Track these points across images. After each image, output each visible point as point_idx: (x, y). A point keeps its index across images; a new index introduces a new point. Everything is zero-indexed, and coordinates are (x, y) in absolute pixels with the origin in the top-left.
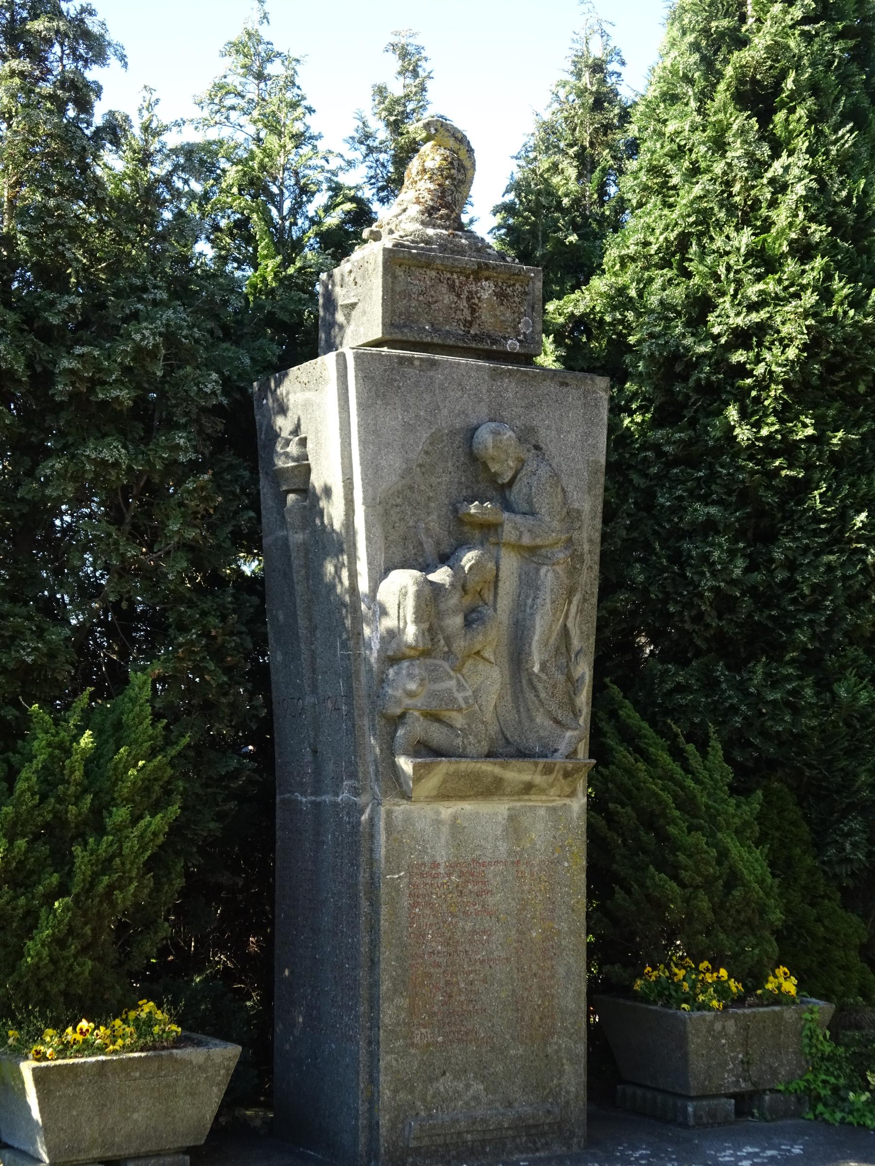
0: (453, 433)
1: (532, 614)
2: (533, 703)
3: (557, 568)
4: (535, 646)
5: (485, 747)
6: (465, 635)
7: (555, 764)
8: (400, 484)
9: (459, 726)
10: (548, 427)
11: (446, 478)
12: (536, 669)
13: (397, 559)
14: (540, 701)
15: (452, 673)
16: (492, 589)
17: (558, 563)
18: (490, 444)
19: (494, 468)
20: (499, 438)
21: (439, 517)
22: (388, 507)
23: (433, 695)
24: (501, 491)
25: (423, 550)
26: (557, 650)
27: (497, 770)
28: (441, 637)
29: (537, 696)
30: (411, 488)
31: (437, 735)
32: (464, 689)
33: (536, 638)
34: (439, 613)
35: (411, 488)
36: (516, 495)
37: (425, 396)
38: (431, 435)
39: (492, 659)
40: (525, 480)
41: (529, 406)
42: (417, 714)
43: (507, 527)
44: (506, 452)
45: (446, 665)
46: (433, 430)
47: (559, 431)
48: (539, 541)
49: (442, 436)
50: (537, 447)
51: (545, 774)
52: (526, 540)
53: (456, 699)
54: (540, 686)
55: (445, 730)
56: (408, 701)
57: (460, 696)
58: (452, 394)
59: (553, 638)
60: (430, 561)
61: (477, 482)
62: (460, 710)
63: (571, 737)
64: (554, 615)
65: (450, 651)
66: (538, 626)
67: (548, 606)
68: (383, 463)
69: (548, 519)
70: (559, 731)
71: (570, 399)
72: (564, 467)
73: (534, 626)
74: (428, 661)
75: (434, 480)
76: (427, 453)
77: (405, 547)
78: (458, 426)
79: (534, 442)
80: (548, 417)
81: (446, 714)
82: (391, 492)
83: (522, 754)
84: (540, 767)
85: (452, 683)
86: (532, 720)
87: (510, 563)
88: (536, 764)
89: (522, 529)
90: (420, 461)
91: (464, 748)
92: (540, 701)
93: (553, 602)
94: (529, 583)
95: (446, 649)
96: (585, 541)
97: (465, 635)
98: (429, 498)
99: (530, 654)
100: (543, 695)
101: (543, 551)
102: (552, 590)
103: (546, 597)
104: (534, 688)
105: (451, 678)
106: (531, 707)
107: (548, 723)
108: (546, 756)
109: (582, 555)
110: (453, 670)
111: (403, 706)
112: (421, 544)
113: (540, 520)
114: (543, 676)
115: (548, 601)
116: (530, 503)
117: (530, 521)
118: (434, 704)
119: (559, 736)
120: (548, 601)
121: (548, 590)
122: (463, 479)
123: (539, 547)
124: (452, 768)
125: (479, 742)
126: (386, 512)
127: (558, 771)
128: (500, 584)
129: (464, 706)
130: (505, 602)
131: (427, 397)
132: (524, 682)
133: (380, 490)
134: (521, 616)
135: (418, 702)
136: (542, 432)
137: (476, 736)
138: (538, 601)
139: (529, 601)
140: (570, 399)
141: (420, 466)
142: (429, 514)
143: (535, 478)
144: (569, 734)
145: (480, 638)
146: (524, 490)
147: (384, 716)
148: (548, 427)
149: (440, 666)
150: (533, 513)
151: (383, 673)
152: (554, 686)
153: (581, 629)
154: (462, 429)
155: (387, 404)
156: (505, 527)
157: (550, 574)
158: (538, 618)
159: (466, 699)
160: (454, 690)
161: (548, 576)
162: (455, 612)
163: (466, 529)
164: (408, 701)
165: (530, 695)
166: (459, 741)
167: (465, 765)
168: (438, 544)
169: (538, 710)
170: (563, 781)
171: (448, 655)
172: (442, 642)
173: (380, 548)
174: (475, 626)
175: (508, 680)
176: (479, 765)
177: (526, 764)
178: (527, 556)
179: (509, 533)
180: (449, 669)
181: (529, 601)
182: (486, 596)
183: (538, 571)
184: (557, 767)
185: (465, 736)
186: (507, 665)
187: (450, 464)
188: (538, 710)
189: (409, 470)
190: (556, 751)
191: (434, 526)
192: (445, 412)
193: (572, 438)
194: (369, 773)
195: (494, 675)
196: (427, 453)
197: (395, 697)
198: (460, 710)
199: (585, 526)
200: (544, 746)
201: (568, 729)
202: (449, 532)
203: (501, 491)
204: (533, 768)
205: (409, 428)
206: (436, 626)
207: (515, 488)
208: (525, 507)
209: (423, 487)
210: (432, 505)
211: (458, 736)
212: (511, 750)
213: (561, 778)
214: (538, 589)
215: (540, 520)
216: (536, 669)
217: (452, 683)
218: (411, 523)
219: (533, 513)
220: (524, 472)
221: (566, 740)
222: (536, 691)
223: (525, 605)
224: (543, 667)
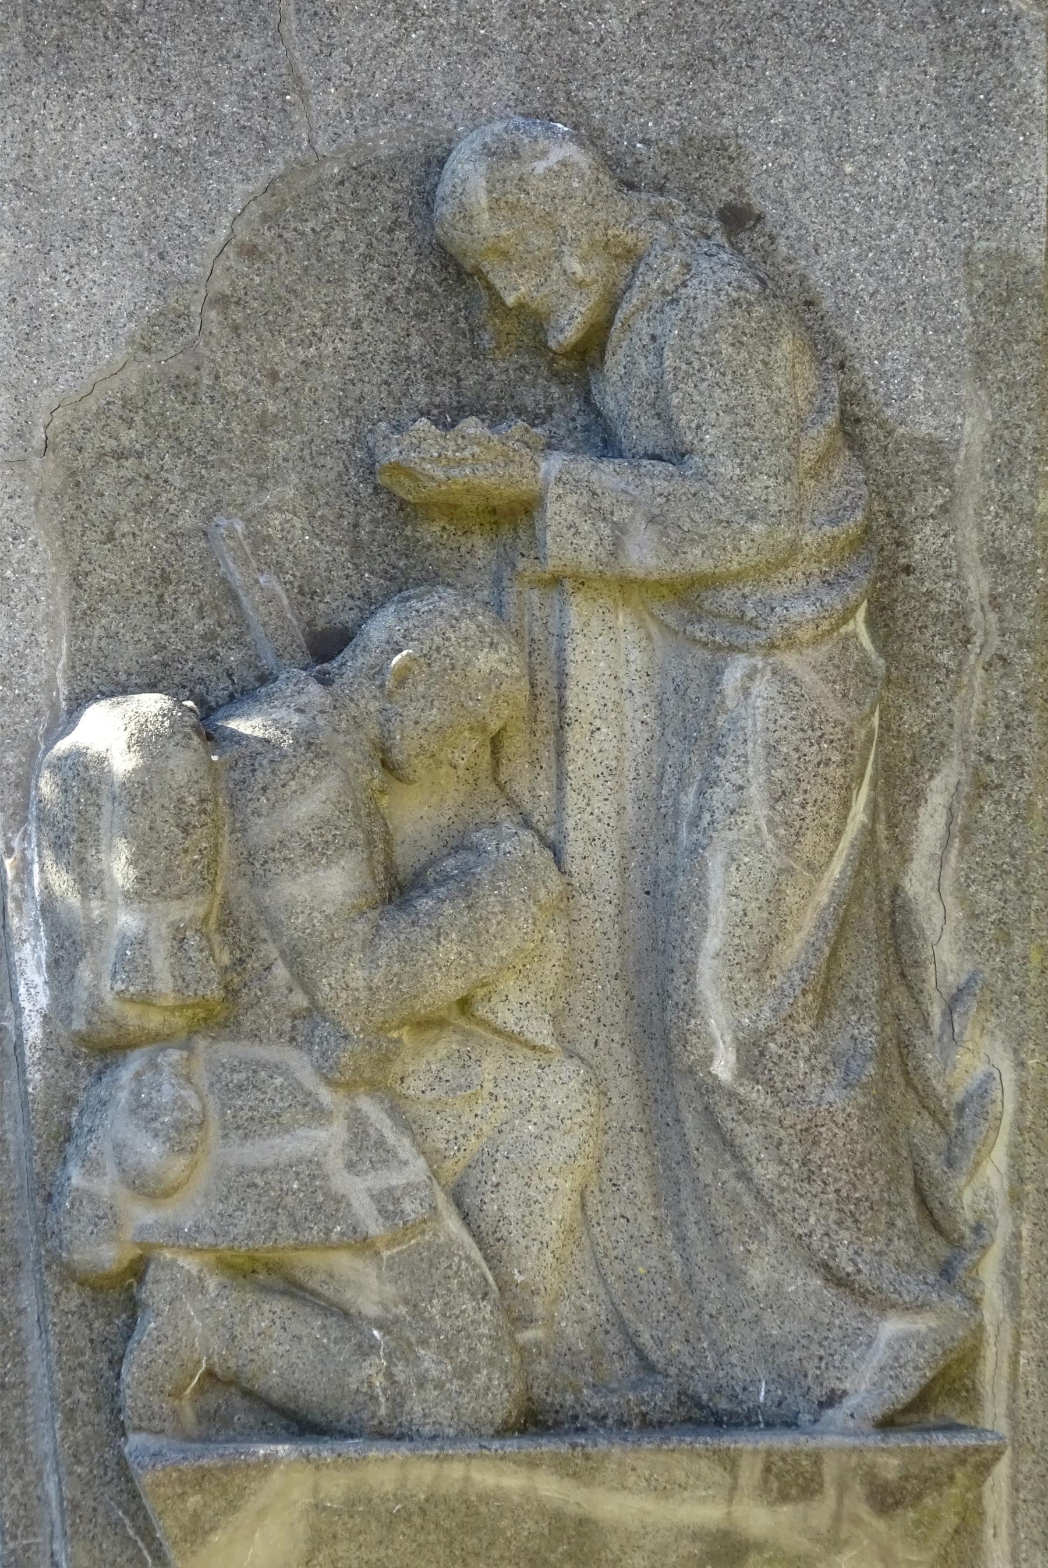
0: (364, 174)
1: (695, 849)
2: (735, 1203)
3: (790, 660)
4: (708, 969)
5: (496, 1394)
6: (370, 944)
7: (817, 1458)
8: (133, 375)
9: (371, 1310)
10: (787, 138)
11: (337, 344)
12: (723, 1066)
13: (127, 658)
14: (758, 1194)
15: (326, 1096)
16: (547, 755)
17: (792, 642)
18: (480, 198)
19: (516, 288)
20: (513, 169)
21: (310, 490)
22: (86, 460)
23: (241, 1185)
24: (568, 380)
25: (241, 620)
26: (826, 990)
27: (550, 1487)
28: (271, 951)
29: (745, 1176)
30: (181, 386)
31: (280, 1347)
32: (385, 1156)
33: (712, 942)
34: (250, 858)
35: (181, 386)
36: (618, 387)
37: (237, 42)
38: (270, 188)
39: (541, 1032)
40: (643, 327)
41: (701, 62)
42: (189, 1263)
43: (560, 512)
44: (548, 222)
45: (300, 1065)
46: (278, 168)
47: (835, 149)
48: (697, 559)
49: (319, 186)
50: (737, 219)
51: (784, 1497)
52: (643, 555)
53: (339, 1200)
54: (750, 1138)
55: (312, 1326)
56: (142, 1216)
57: (358, 1190)
58: (359, 30)
59: (798, 941)
60: (268, 661)
61: (476, 352)
62: (362, 1244)
63: (904, 1340)
64: (788, 848)
65: (314, 1011)
66: (716, 894)
67: (759, 812)
68: (62, 297)
69: (729, 469)
70: (850, 1315)
71: (880, 31)
72: (862, 283)
73: (700, 897)
74: (227, 1051)
75: (286, 356)
76: (250, 252)
77: (162, 610)
78: (384, 149)
79: (724, 195)
80: (782, 100)
81: (312, 1265)
82: (91, 403)
83: (704, 1415)
84: (750, 1472)
85: (328, 1139)
86: (733, 1275)
87: (608, 659)
88: (730, 1462)
89: (623, 514)
90: (222, 284)
91: (398, 1401)
92: (758, 1194)
93: (779, 796)
94: (689, 728)
95: (299, 1000)
96: (971, 558)
97: (370, 944)
98: (264, 424)
99: (691, 1008)
100: (766, 1172)
101: (728, 598)
102: (771, 749)
103: (748, 780)
104: (728, 1144)
105: (320, 1114)
106: (725, 1219)
107: (803, 1285)
108: (790, 1424)
109: (961, 613)
110: (332, 1083)
111: (129, 1234)
112: (232, 596)
113: (701, 476)
114: (757, 1096)
115: (754, 791)
116: (665, 418)
117: (658, 478)
118: (243, 1222)
119: (849, 1339)
120: (754, 791)
121: (755, 750)
122: (416, 343)
123: (712, 582)
124: (336, 1486)
125: (464, 1373)
126: (75, 481)
127: (842, 1488)
128: (574, 736)
129: (375, 1227)
130: (596, 812)
131: (251, 50)
132: (690, 1121)
133: (46, 398)
134: (665, 858)
135: (184, 1211)
136: (761, 156)
137: (447, 1349)
138: (718, 795)
139: (688, 799)
140: (880, 31)
141: (222, 301)
142: (262, 481)
143: (674, 314)
144: (891, 1327)
145: (449, 949)
146: (643, 369)
147: (70, 1275)
148: (787, 138)
149: (276, 1068)
150: (676, 455)
151: (69, 1101)
152: (809, 1135)
153: (964, 899)
154: (406, 158)
155: (77, 79)
156: (551, 508)
157: (761, 687)
158: (715, 861)
159: (387, 1203)
160: (334, 1163)
161: (751, 695)
162: (318, 851)
163: (430, 531)
164: (142, 1216)
165: (714, 1172)
166: (372, 1371)
167: (387, 1472)
168: (306, 594)
169: (755, 1232)
170: (879, 1525)
171: (308, 1024)
172: (281, 972)
173: (49, 619)
174: (425, 904)
175: (631, 1114)
176: (456, 1471)
177: (685, 1458)
178: (670, 619)
179: (568, 535)
180: (308, 1077)
181: (688, 799)
182: (520, 787)
183: (714, 675)
184: (829, 1471)
185: (402, 1351)
186: (627, 1059)
187: (354, 291)
188: (755, 1232)
189: (171, 322)
190: (832, 1399)
191: (281, 531)
192: (331, 98)
193: (892, 171)
194: (42, 1500)
195: (556, 1098)
196: (250, 252)
197: (93, 1198)
198: (362, 1244)
199: (971, 502)
200: (788, 1379)
201: (886, 1306)
202: (356, 546)
203: (568, 380)
204: (718, 1475)
205: (169, 164)
206: (246, 909)
207: (615, 364)
208: (654, 437)
209: (235, 382)
210: (279, 446)
211: (366, 1349)
212: (659, 1398)
213: (863, 1510)
214: (717, 748)
215: (701, 476)
216: (723, 1066)
217: (328, 1139)
218: (187, 520)
219: (676, 455)
220: (635, 298)
221: (879, 1355)
222: (738, 1157)
223: (677, 813)
224: (753, 1058)
